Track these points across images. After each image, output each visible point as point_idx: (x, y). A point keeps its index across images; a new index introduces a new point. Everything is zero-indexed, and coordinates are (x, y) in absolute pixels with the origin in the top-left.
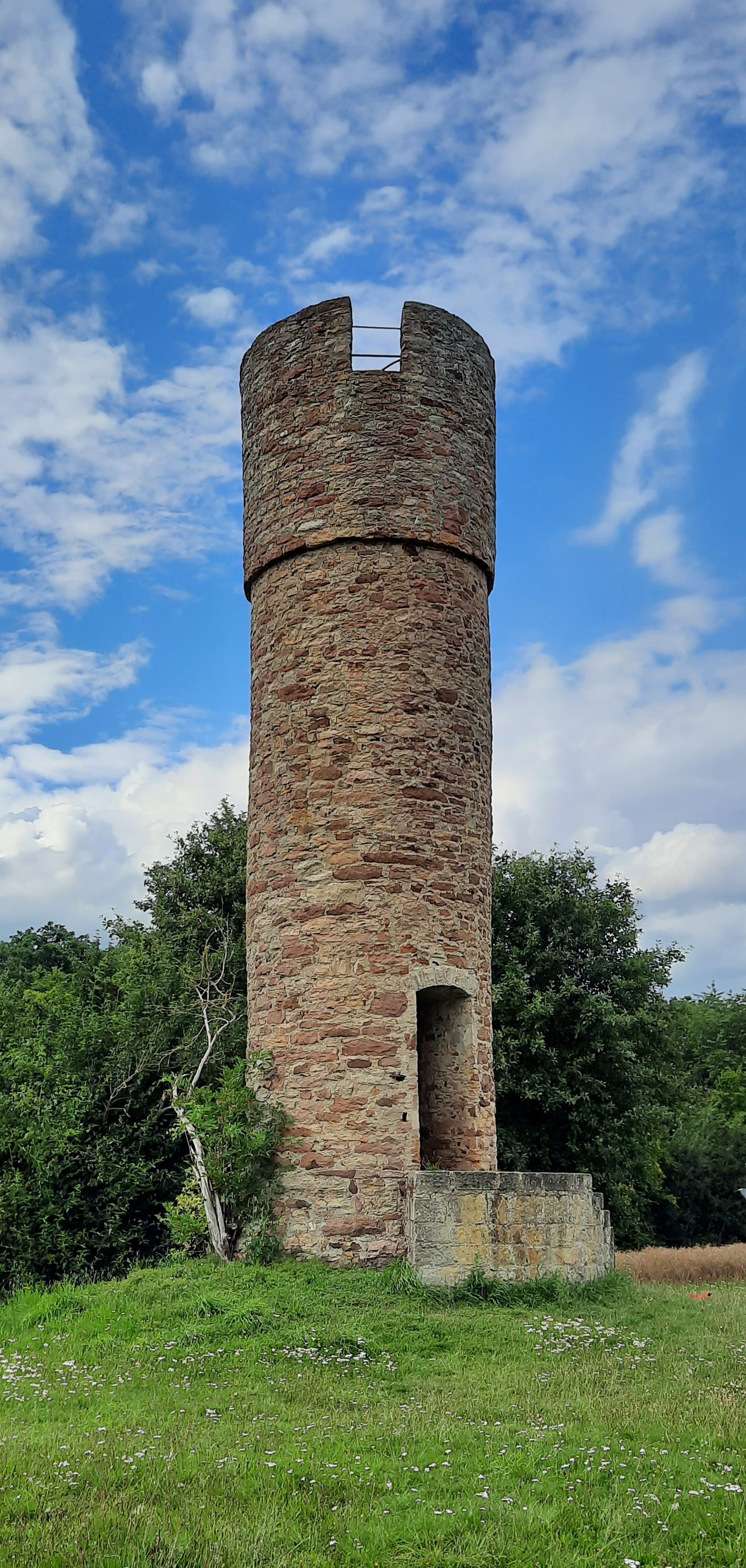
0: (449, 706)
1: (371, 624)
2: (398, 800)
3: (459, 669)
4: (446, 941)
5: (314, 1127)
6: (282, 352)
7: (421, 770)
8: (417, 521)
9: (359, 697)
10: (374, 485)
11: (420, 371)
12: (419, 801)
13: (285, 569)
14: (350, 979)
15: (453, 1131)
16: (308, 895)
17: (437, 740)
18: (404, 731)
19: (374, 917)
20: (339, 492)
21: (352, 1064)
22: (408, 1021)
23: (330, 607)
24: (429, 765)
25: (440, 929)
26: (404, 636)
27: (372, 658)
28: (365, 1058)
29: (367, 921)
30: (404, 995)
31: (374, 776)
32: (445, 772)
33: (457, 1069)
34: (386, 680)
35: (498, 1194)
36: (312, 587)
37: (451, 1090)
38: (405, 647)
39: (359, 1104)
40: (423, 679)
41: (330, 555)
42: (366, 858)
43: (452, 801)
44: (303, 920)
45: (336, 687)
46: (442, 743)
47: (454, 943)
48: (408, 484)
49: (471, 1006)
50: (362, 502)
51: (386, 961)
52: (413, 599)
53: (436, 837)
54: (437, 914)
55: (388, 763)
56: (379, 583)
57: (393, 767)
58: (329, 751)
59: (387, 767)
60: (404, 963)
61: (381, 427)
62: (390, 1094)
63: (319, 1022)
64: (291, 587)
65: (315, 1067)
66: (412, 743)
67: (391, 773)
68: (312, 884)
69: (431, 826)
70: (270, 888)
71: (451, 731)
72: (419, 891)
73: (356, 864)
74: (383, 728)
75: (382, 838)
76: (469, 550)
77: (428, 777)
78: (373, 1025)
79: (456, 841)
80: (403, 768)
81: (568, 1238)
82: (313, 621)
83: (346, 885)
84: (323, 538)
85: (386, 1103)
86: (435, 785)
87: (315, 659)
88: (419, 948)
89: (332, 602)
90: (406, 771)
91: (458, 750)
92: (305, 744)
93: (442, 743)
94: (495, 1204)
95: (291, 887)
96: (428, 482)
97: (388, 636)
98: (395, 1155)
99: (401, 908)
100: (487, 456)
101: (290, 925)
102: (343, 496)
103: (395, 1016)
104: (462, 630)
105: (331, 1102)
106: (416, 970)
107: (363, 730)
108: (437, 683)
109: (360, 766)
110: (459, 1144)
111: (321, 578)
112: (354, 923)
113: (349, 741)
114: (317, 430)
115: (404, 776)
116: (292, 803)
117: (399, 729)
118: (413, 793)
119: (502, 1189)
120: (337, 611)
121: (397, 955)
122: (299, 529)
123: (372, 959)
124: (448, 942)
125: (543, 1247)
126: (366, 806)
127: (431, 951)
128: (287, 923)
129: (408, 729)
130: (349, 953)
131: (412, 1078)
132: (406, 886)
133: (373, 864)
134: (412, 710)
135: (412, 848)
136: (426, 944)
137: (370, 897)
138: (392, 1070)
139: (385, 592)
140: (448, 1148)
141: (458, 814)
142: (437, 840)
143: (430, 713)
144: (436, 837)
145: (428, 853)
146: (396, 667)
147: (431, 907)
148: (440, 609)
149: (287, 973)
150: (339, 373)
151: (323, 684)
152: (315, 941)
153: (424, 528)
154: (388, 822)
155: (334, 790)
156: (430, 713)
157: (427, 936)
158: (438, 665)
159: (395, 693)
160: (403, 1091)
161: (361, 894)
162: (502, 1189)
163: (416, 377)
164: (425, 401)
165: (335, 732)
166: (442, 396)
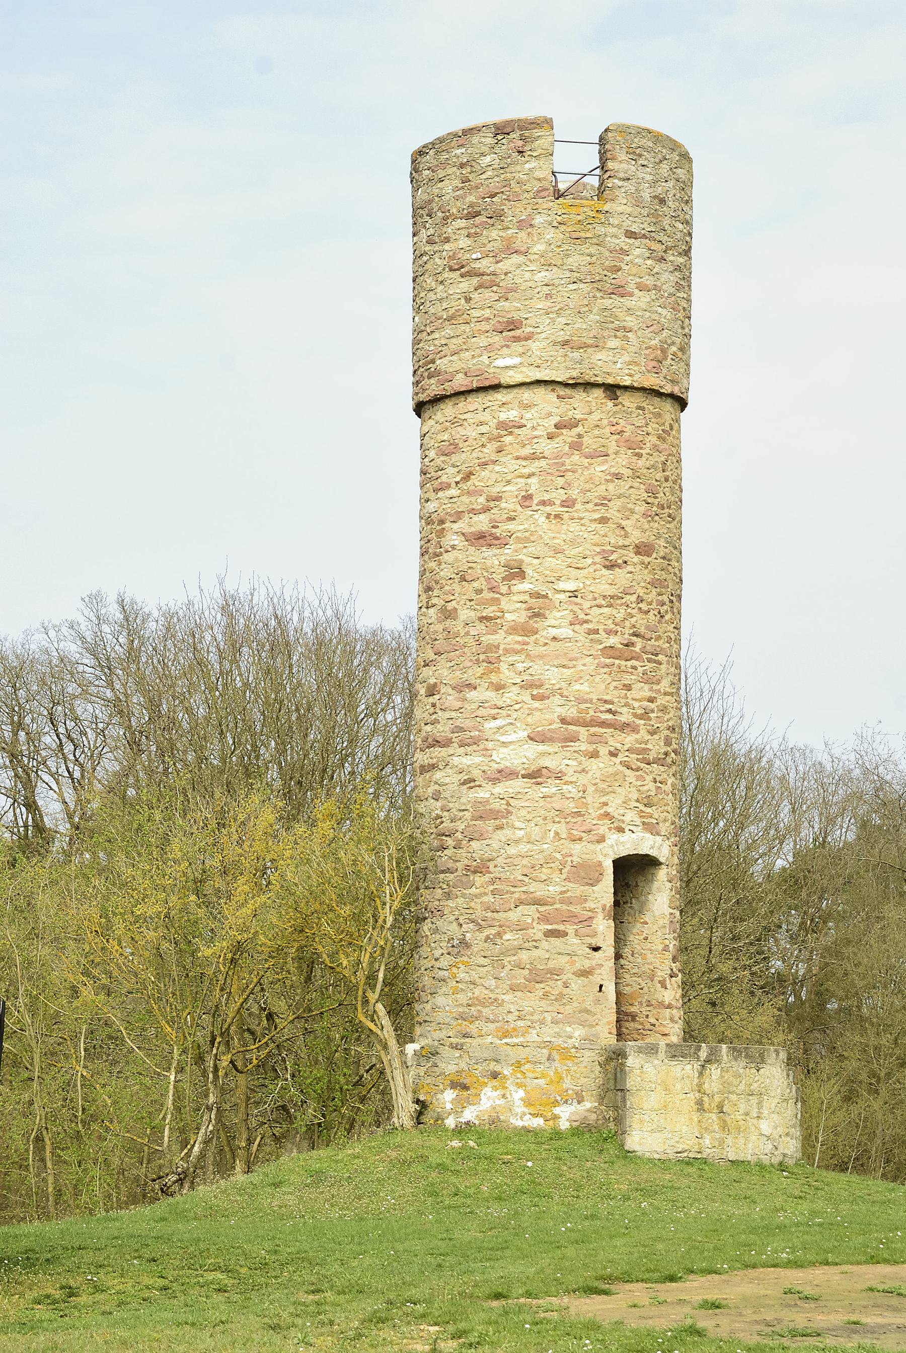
0: (647, 559)
1: (571, 473)
2: (597, 661)
3: (657, 518)
4: (642, 807)
5: (506, 998)
6: (474, 164)
7: (619, 629)
8: (619, 365)
9: (558, 551)
10: (576, 326)
11: (625, 201)
12: (617, 662)
13: (476, 402)
14: (545, 846)
15: (641, 1003)
16: (501, 756)
17: (635, 596)
18: (605, 588)
19: (571, 782)
20: (538, 330)
21: (549, 934)
22: (604, 891)
23: (527, 451)
24: (627, 624)
25: (635, 795)
26: (603, 487)
27: (570, 510)
28: (561, 927)
29: (565, 787)
30: (600, 864)
31: (571, 634)
32: (642, 630)
33: (646, 939)
34: (583, 533)
35: (703, 1066)
36: (507, 427)
37: (639, 960)
38: (605, 499)
39: (556, 973)
40: (623, 533)
41: (526, 395)
42: (563, 721)
43: (649, 660)
44: (495, 781)
45: (532, 538)
46: (640, 600)
47: (649, 810)
48: (611, 326)
49: (662, 874)
50: (565, 343)
51: (583, 828)
52: (612, 447)
53: (633, 699)
54: (633, 780)
55: (586, 622)
56: (579, 429)
57: (591, 626)
58: (524, 606)
59: (585, 626)
60: (601, 832)
61: (584, 263)
62: (587, 964)
63: (513, 889)
64: (482, 424)
65: (507, 936)
66: (612, 600)
67: (590, 632)
68: (504, 744)
69: (628, 687)
70: (455, 745)
71: (649, 586)
72: (615, 755)
73: (552, 727)
74: (581, 585)
75: (580, 700)
76: (667, 389)
77: (626, 636)
78: (569, 894)
79: (652, 702)
80: (601, 627)
81: (765, 1112)
82: (508, 465)
83: (541, 748)
84: (519, 378)
85: (585, 973)
86: (633, 644)
87: (511, 506)
88: (616, 815)
89: (528, 446)
90: (605, 630)
91: (654, 606)
92: (497, 596)
93: (640, 600)
94: (701, 1074)
95: (482, 747)
96: (630, 321)
97: (588, 486)
98: (593, 1026)
99: (598, 775)
100: (685, 281)
101: (480, 786)
102: (543, 335)
103: (592, 885)
104: (660, 475)
105: (526, 972)
106: (613, 838)
107: (562, 585)
108: (636, 537)
109: (557, 623)
110: (647, 1016)
111: (516, 419)
112: (550, 788)
113: (545, 596)
114: (516, 259)
115: (602, 635)
116: (482, 657)
117: (599, 586)
118: (611, 653)
119: (708, 1061)
120: (533, 457)
121: (594, 822)
122: (494, 364)
123: (570, 826)
124: (644, 809)
125: (743, 1117)
126: (564, 666)
127: (627, 818)
128: (477, 783)
129: (607, 586)
130: (545, 819)
131: (609, 950)
132: (603, 751)
133: (570, 727)
134: (611, 566)
135: (610, 711)
136: (622, 812)
137: (568, 762)
138: (589, 940)
139: (585, 439)
140: (634, 1020)
141: (654, 674)
142: (634, 702)
143: (629, 568)
144: (633, 699)
145: (625, 716)
146: (595, 520)
147: (628, 772)
148: (640, 456)
149: (476, 835)
150: (540, 201)
151: (519, 534)
152: (508, 804)
153: (627, 371)
154: (586, 684)
155: (529, 647)
156: (629, 568)
157: (624, 803)
158: (637, 516)
159: (595, 548)
160: (600, 962)
161: (554, 758)
162: (708, 1061)
163: (621, 208)
164: (630, 234)
165: (532, 586)
166: (645, 225)
